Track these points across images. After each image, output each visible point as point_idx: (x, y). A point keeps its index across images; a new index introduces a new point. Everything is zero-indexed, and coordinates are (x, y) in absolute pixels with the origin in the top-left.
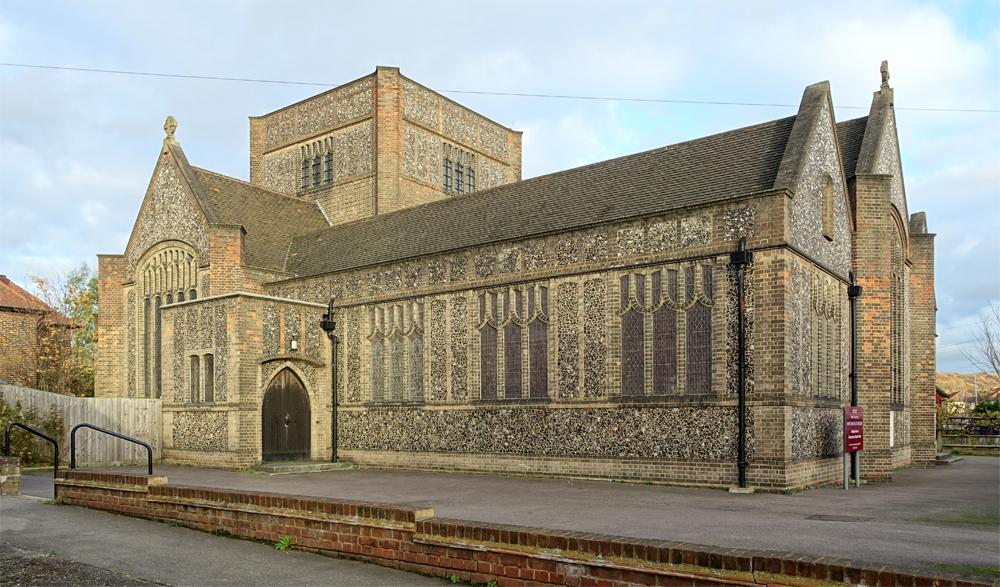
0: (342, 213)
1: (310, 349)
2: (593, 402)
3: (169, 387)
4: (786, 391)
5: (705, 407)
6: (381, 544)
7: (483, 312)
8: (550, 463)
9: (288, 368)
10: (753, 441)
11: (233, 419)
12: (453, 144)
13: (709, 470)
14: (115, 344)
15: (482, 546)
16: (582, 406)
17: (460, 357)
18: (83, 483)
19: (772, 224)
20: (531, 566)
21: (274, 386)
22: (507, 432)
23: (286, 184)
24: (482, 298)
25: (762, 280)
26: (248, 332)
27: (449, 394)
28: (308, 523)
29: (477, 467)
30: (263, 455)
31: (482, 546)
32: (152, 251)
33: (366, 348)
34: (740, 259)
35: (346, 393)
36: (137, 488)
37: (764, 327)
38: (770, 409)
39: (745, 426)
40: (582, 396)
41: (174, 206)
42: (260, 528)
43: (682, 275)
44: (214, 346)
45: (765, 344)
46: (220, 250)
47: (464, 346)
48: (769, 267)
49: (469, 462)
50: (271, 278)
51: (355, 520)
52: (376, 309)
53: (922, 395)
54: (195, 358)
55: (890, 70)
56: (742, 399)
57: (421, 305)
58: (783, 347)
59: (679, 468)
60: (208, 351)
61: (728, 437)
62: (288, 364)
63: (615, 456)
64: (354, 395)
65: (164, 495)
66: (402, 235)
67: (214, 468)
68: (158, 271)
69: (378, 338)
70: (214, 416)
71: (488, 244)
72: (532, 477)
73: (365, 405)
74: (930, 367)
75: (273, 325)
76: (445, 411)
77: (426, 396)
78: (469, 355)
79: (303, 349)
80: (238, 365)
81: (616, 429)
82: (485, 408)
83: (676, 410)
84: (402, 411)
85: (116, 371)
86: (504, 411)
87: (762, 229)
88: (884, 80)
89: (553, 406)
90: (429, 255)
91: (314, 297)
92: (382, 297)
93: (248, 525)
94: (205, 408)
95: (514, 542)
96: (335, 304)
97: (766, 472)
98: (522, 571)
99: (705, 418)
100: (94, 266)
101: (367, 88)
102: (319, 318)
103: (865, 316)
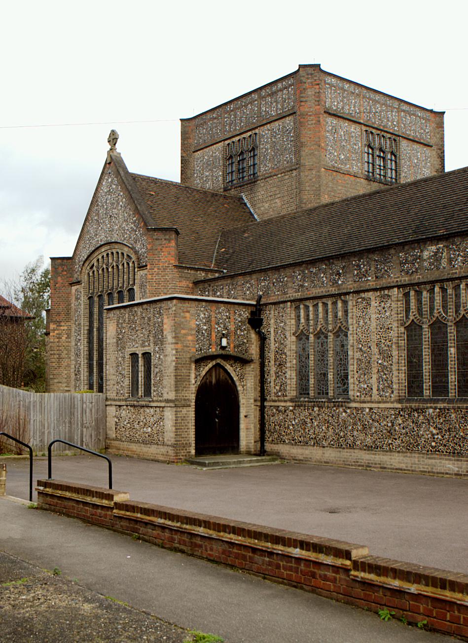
0: (267, 205)
1: (239, 346)
3: (112, 382)
6: (320, 576)
7: (408, 310)
9: (218, 365)
11: (169, 415)
12: (374, 131)
14: (64, 338)
15: (413, 588)
17: (386, 355)
18: (59, 493)
20: (459, 612)
21: (206, 382)
22: (435, 431)
23: (211, 178)
24: (407, 295)
27: (375, 391)
28: (254, 550)
29: (403, 466)
30: (196, 449)
31: (413, 588)
32: (96, 254)
33: (291, 342)
35: (273, 387)
36: (105, 502)
41: (115, 211)
42: (211, 550)
44: (152, 345)
46: (156, 252)
47: (389, 343)
49: (396, 460)
50: (202, 275)
51: (297, 552)
52: (302, 306)
54: (134, 355)
57: (345, 303)
60: (147, 349)
62: (219, 361)
64: (280, 391)
65: (128, 511)
66: (326, 230)
67: (152, 460)
68: (100, 272)
69: (301, 336)
70: (152, 410)
71: (413, 242)
73: (291, 400)
75: (205, 324)
76: (371, 409)
77: (351, 393)
78: (395, 353)
79: (232, 346)
80: (174, 364)
84: (328, 407)
85: (64, 363)
86: (431, 411)
90: (353, 254)
91: (245, 292)
92: (308, 294)
93: (200, 546)
94: (144, 403)
95: (443, 587)
96: (263, 301)
98: (450, 616)
100: (47, 264)
101: (290, 85)
102: (246, 314)
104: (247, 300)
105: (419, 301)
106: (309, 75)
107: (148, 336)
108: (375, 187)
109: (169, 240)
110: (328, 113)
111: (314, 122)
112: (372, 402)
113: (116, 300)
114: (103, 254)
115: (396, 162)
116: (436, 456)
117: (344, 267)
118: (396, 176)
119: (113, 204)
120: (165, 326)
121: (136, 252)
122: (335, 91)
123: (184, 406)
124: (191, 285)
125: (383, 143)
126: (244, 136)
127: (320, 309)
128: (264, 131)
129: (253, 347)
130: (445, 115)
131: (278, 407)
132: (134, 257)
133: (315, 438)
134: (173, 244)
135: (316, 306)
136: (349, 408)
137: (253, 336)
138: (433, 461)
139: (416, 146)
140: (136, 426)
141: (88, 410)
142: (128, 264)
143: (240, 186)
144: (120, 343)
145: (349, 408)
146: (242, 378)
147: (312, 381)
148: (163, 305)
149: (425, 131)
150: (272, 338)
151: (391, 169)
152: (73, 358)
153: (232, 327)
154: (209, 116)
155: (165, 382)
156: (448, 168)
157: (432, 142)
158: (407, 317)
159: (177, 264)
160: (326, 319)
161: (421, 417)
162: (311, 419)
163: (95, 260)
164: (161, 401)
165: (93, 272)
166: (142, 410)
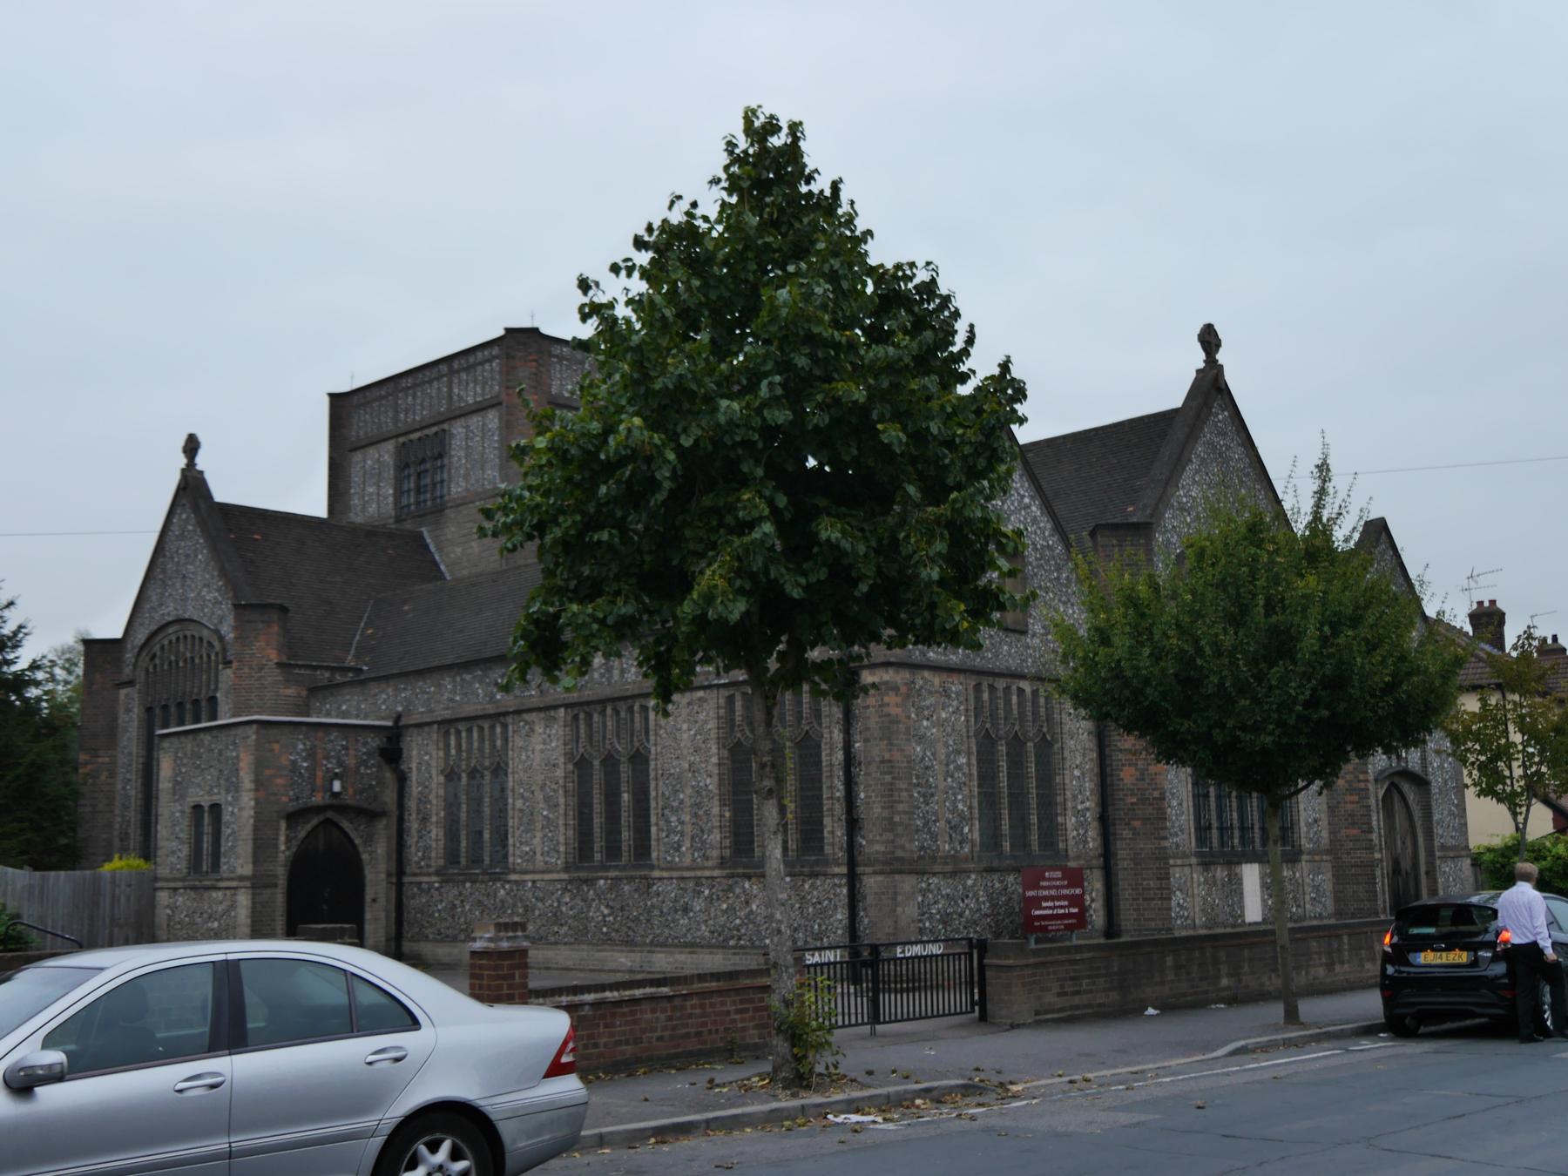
0: (459, 550)
1: (361, 792)
9: (328, 821)
14: (103, 778)
22: (606, 912)
23: (376, 500)
26: (267, 772)
32: (160, 636)
35: (414, 854)
37: (873, 768)
57: (505, 726)
60: (216, 799)
62: (329, 814)
63: (723, 946)
69: (451, 775)
74: (1362, 785)
75: (305, 760)
76: (534, 882)
79: (351, 791)
81: (724, 906)
89: (656, 874)
96: (404, 721)
102: (375, 742)
105: (589, 725)
112: (551, 872)
119: (187, 556)
120: (242, 764)
121: (221, 638)
123: (267, 886)
124: (304, 693)
126: (427, 432)
127: (475, 735)
128: (458, 429)
132: (216, 643)
134: (275, 629)
135: (470, 731)
140: (199, 920)
141: (123, 899)
142: (209, 656)
144: (179, 788)
146: (369, 839)
147: (464, 843)
148: (240, 731)
152: (117, 812)
153: (351, 762)
154: (376, 393)
155: (239, 850)
159: (285, 660)
160: (481, 750)
166: (206, 895)
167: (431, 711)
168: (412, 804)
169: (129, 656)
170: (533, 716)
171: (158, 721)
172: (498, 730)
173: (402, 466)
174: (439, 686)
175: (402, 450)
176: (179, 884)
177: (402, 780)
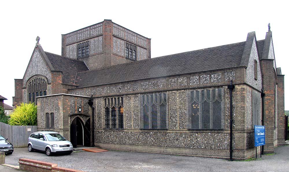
2: (182, 131)
4: (245, 128)
5: (219, 133)
8: (167, 150)
9: (78, 117)
10: (235, 144)
12: (129, 43)
13: (220, 152)
16: (178, 132)
19: (240, 77)
23: (72, 53)
25: (237, 94)
34: (231, 88)
38: (240, 134)
39: (232, 139)
40: (178, 129)
43: (211, 92)
45: (238, 114)
48: (240, 90)
50: (70, 88)
53: (281, 124)
55: (271, 26)
56: (231, 131)
57: (122, 98)
58: (244, 115)
59: (214, 152)
60: (52, 112)
61: (227, 142)
62: (78, 116)
63: (189, 148)
72: (160, 153)
76: (131, 132)
79: (83, 111)
81: (189, 139)
82: (145, 132)
83: (210, 134)
84: (116, 131)
86: (152, 133)
87: (238, 78)
88: (269, 28)
89: (168, 131)
97: (239, 153)
99: (218, 136)
102: (87, 101)
103: (266, 102)
104: (87, 96)
106: (108, 23)
107: (53, 107)
108: (129, 61)
109: (59, 75)
110: (114, 36)
111: (109, 39)
112: (132, 130)
113: (39, 95)
114: (34, 79)
115: (135, 54)
116: (153, 147)
117: (122, 86)
118: (135, 58)
120: (59, 104)
121: (47, 79)
122: (116, 29)
124: (67, 90)
125: (132, 47)
128: (92, 41)
129: (90, 111)
130: (151, 40)
131: (99, 131)
133: (112, 141)
136: (124, 132)
137: (90, 108)
138: (152, 148)
139: (142, 49)
142: (44, 82)
143: (83, 58)
145: (124, 132)
149: (143, 43)
150: (97, 109)
151: (134, 55)
156: (152, 57)
157: (147, 48)
158: (144, 103)
161: (148, 135)
162: (111, 135)
163: (31, 80)
164: (58, 129)
165: (31, 85)
167: (101, 94)
168: (96, 114)
169: (24, 83)
170: (130, 96)
171: (36, 95)
172: (120, 98)
173: (78, 48)
174: (103, 89)
175: (78, 45)
176: (44, 130)
177: (93, 109)
